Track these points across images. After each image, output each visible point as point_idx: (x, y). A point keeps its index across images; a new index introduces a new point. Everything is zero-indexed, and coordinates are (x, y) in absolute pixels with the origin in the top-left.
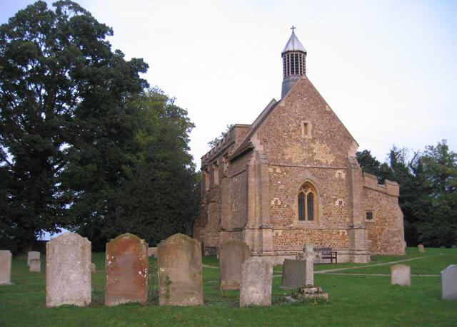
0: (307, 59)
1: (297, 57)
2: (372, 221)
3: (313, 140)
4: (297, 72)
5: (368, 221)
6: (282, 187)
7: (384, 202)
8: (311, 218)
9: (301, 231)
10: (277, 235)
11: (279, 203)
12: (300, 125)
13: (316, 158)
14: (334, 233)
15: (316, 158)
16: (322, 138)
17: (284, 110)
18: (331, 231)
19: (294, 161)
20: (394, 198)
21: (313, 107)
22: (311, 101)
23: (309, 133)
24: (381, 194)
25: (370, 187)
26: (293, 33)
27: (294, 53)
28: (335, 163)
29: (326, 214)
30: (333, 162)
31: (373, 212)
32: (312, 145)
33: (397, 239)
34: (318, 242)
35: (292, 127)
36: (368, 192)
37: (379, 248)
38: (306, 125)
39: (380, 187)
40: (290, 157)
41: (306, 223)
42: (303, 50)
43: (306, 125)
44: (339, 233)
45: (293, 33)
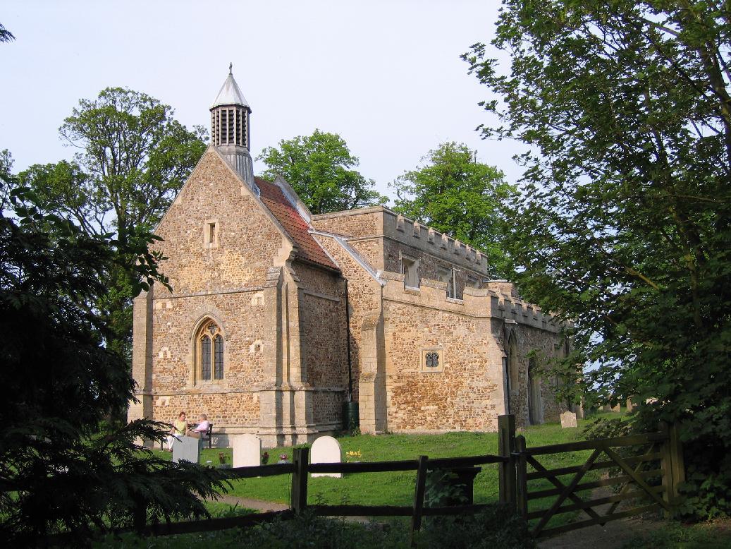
0: (253, 118)
1: (231, 115)
2: (438, 369)
3: (220, 250)
4: (231, 139)
5: (428, 369)
6: (173, 330)
7: (461, 331)
8: (219, 374)
9: (196, 396)
10: (163, 404)
11: (169, 356)
12: (202, 229)
13: (224, 277)
14: (244, 398)
15: (224, 277)
16: (234, 243)
17: (180, 209)
18: (239, 395)
19: (191, 287)
20: (481, 321)
21: (223, 195)
22: (221, 186)
23: (216, 238)
24: (455, 316)
25: (431, 304)
26: (231, 74)
27: (227, 109)
28: (622, 259)
29: (235, 368)
30: (250, 281)
31: (439, 353)
32: (219, 258)
33: (489, 402)
34: (217, 414)
35: (190, 234)
36: (430, 314)
37: (451, 421)
38: (213, 226)
39: (452, 303)
40: (187, 281)
41: (212, 385)
42: (245, 104)
43: (213, 226)
44: (251, 398)
45: (231, 74)
